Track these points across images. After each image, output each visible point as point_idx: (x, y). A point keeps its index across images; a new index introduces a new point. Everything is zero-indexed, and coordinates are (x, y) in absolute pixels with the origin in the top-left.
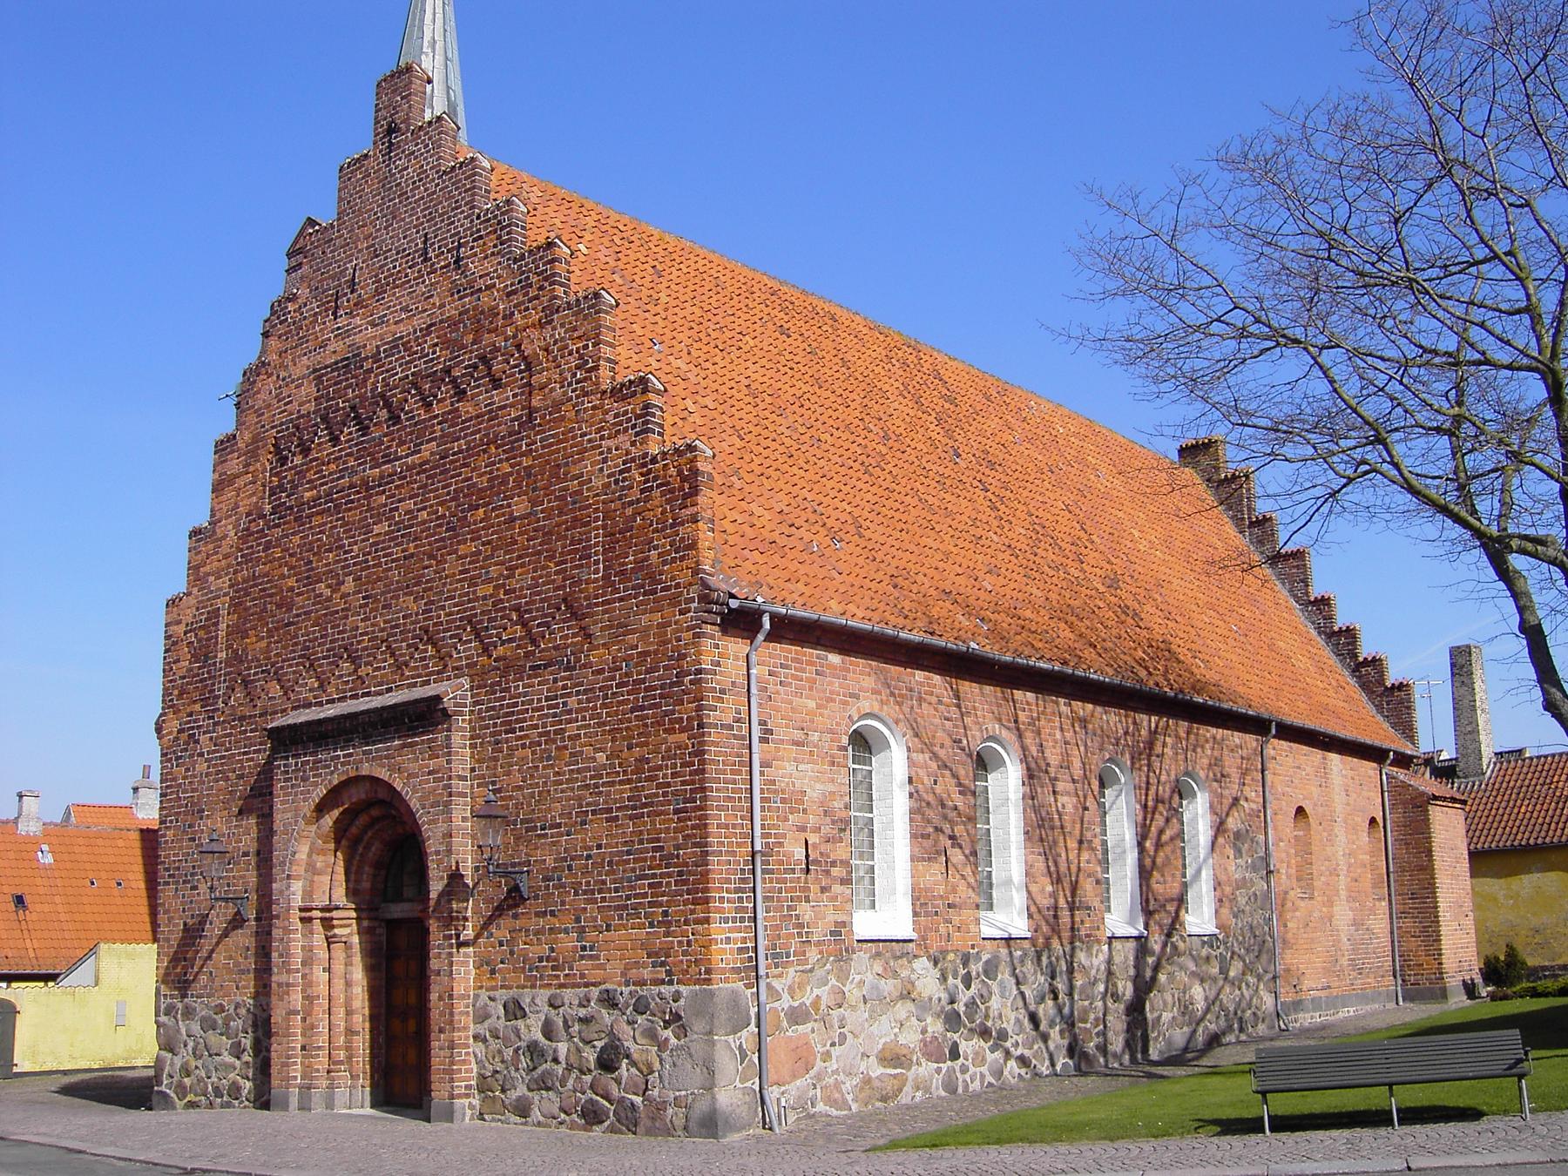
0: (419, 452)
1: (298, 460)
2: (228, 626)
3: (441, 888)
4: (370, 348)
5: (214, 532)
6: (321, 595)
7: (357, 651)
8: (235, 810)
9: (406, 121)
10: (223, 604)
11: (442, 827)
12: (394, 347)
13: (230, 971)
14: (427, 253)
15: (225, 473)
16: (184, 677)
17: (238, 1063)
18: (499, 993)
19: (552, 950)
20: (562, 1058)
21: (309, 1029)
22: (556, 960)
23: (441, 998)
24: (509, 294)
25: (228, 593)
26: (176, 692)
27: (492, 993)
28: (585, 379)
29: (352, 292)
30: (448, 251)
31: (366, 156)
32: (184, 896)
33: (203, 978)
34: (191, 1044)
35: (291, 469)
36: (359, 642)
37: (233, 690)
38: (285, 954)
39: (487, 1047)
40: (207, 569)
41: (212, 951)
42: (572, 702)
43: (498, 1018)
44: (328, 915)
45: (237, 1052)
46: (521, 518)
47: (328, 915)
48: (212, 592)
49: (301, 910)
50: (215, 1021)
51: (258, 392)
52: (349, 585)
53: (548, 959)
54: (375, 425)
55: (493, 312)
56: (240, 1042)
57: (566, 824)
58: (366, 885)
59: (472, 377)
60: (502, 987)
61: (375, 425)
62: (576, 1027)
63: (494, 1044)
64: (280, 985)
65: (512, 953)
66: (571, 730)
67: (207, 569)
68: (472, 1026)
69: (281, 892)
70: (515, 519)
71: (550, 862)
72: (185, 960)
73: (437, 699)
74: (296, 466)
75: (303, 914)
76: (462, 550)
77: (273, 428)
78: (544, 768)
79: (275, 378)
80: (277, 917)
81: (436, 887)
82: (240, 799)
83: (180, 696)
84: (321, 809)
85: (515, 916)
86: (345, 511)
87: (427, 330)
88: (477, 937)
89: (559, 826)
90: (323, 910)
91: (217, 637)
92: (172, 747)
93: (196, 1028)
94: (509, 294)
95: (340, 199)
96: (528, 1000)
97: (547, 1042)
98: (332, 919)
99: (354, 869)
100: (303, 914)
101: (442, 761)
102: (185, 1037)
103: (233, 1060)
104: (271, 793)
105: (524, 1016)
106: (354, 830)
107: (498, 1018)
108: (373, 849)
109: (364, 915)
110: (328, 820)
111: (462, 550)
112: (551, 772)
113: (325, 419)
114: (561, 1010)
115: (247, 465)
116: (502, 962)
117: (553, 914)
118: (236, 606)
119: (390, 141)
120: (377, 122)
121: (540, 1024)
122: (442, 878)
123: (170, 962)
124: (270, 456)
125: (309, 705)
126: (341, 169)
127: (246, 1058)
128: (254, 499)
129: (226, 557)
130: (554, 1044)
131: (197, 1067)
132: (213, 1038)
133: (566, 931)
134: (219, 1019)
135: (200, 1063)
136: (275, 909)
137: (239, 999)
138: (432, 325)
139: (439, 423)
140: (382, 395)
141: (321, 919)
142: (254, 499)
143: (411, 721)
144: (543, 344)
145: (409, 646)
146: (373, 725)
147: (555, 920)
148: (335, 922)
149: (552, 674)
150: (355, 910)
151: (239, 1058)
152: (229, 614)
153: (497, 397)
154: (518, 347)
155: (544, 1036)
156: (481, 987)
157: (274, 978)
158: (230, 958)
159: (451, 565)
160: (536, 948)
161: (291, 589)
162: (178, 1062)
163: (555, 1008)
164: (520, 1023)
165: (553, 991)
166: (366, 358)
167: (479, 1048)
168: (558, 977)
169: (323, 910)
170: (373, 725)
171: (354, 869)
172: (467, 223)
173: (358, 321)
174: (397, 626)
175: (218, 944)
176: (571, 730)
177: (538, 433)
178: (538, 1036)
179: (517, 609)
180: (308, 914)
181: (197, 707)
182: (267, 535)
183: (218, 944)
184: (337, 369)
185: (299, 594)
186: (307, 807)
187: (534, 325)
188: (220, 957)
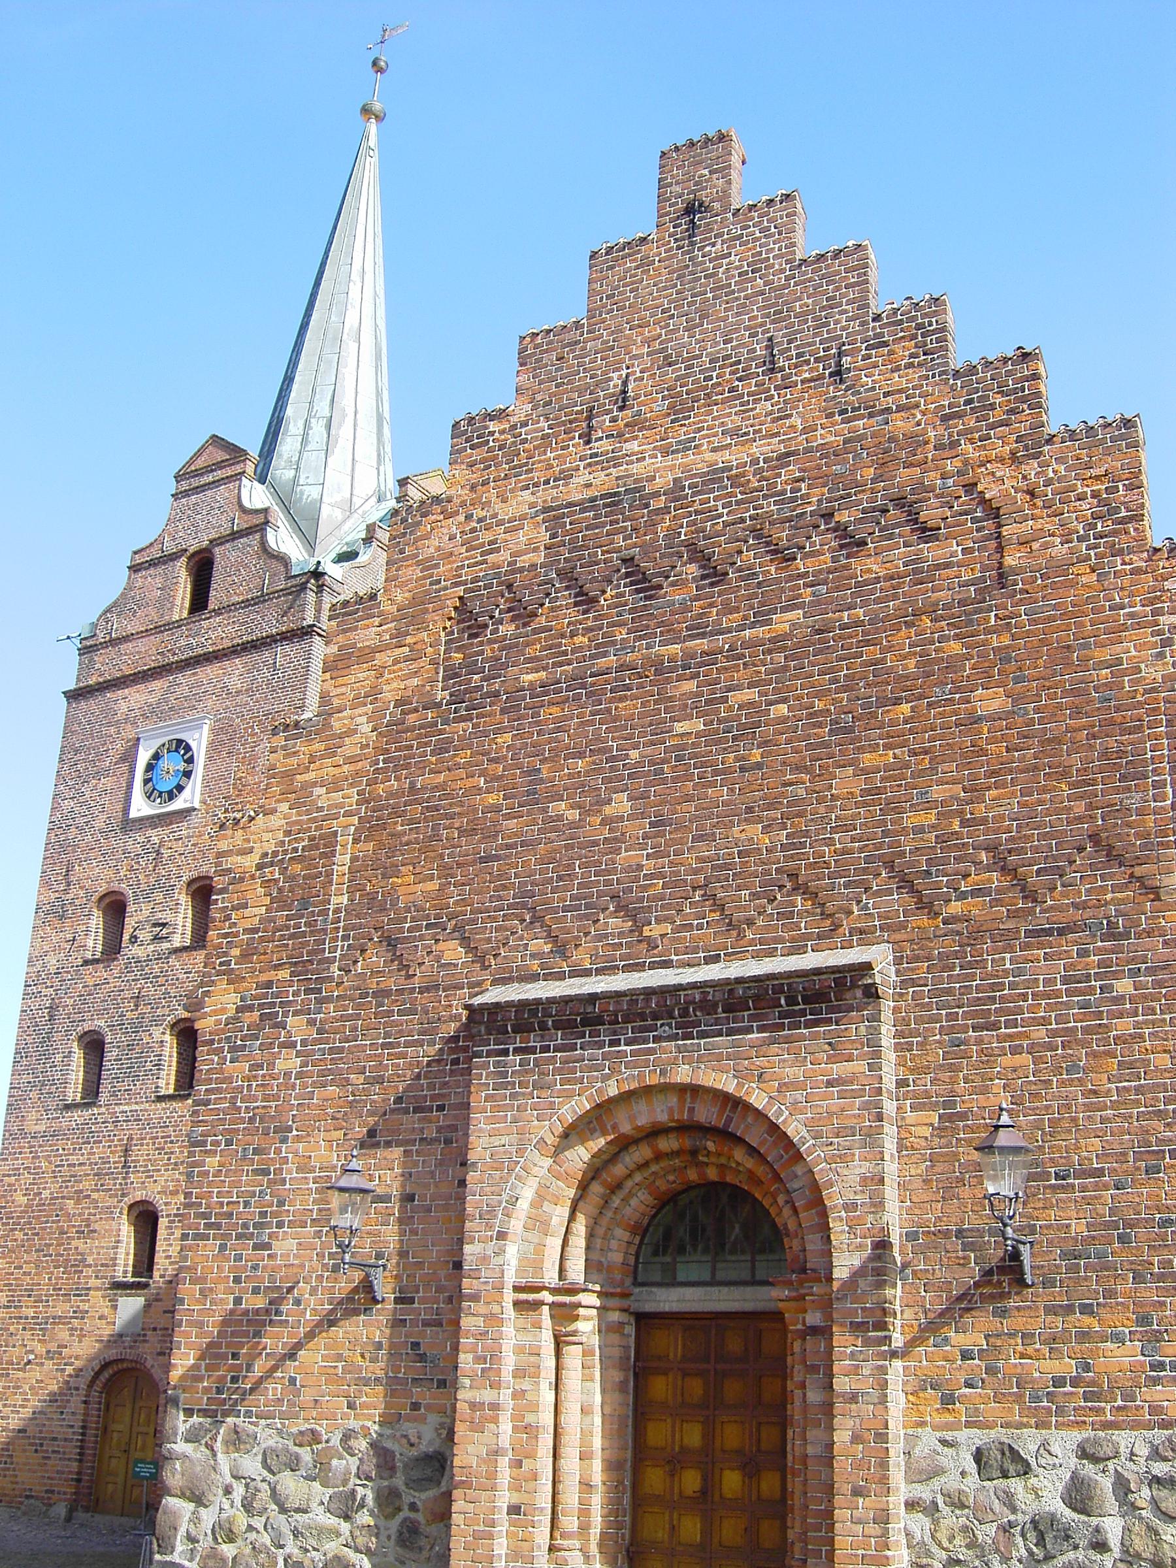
0: (769, 622)
1: (507, 629)
2: (354, 859)
3: (857, 1263)
4: (663, 481)
5: (327, 725)
6: (560, 818)
7: (641, 900)
8: (360, 1131)
9: (725, 196)
10: (346, 829)
11: (859, 1168)
12: (713, 481)
13: (333, 1378)
14: (773, 362)
15: (354, 646)
16: (255, 930)
17: (345, 1527)
18: (962, 1435)
19: (1087, 1367)
20: (1114, 1541)
21: (524, 1481)
22: (1092, 1383)
23: (856, 1439)
24: (945, 418)
25: (358, 812)
26: (236, 952)
27: (948, 1436)
28: (1114, 533)
29: (621, 409)
30: (817, 360)
31: (643, 240)
32: (239, 1258)
33: (273, 1389)
34: (239, 1491)
35: (491, 642)
36: (645, 888)
37: (363, 951)
38: (490, 1359)
39: (936, 1522)
40: (311, 776)
41: (298, 1346)
42: (1124, 986)
43: (963, 1474)
44: (567, 1299)
45: (346, 1507)
46: (991, 718)
47: (567, 1299)
48: (321, 809)
49: (517, 1289)
50: (298, 1458)
51: (426, 537)
52: (621, 804)
53: (1075, 1382)
54: (673, 584)
55: (916, 441)
56: (353, 1492)
57: (1113, 1171)
58: (617, 1257)
59: (878, 523)
60: (968, 1425)
61: (673, 584)
62: (1146, 1492)
63: (950, 1520)
64: (473, 1406)
65: (991, 1371)
66: (1124, 1026)
67: (311, 776)
68: (903, 1485)
69: (485, 1259)
70: (980, 719)
71: (1078, 1228)
72: (235, 1356)
73: (867, 967)
74: (504, 638)
75: (523, 1296)
76: (867, 759)
77: (456, 584)
78: (1062, 1083)
79: (461, 518)
80: (475, 1298)
81: (845, 1264)
82: (371, 1113)
83: (245, 956)
84: (571, 1134)
85: (1003, 1313)
86: (611, 700)
87: (784, 458)
88: (911, 1344)
89: (1100, 1173)
90: (555, 1291)
91: (329, 874)
92: (223, 1031)
93: (252, 1465)
94: (945, 418)
95: (592, 293)
96: (1033, 1447)
97: (1075, 1516)
98: (580, 1305)
99: (600, 1231)
100: (523, 1296)
101: (861, 1066)
102: (229, 1479)
103: (332, 1521)
104: (467, 1106)
105: (1026, 1470)
106: (619, 1170)
107: (963, 1474)
108: (634, 1202)
109: (614, 1302)
110: (581, 1155)
111: (867, 759)
112: (1076, 1090)
113: (567, 576)
114: (1111, 1465)
115: (399, 634)
116: (969, 1385)
117: (1087, 1310)
118: (369, 829)
119: (692, 221)
120: (661, 198)
121: (1060, 1487)
122: (860, 1247)
123: (202, 1358)
124: (448, 624)
125: (534, 978)
126: (594, 255)
127: (365, 1518)
128: (415, 681)
129: (350, 760)
130: (1094, 1521)
131: (250, 1528)
132: (289, 1483)
133: (1118, 1339)
134: (306, 1454)
135: (258, 1523)
136: (468, 1285)
137: (353, 1424)
138: (788, 454)
139: (806, 585)
140: (690, 545)
141: (552, 1305)
142: (415, 681)
143: (792, 1001)
144: (1022, 485)
145: (755, 896)
146: (707, 1007)
147: (1087, 1320)
148: (581, 1311)
149: (1076, 943)
150: (600, 1294)
151: (347, 1518)
152: (356, 841)
153: (930, 552)
154: (970, 487)
155: (1074, 1510)
156: (922, 1424)
157: (461, 1395)
158: (339, 1357)
159: (845, 782)
160: (1047, 1365)
161: (496, 809)
162: (208, 1517)
163: (1095, 1459)
164: (1016, 1485)
165: (1088, 1433)
166: (656, 495)
167: (919, 1524)
168: (1099, 1411)
169: (555, 1291)
170: (707, 1007)
171: (600, 1231)
172: (855, 326)
173: (634, 446)
174: (726, 867)
175: (311, 1335)
176: (1124, 1026)
177: (1021, 602)
178: (1055, 1505)
179: (991, 848)
180: (531, 1297)
181: (284, 974)
182: (441, 732)
183: (311, 1335)
184: (592, 508)
185: (508, 817)
186: (548, 1130)
187: (1001, 460)
188: (313, 1357)
